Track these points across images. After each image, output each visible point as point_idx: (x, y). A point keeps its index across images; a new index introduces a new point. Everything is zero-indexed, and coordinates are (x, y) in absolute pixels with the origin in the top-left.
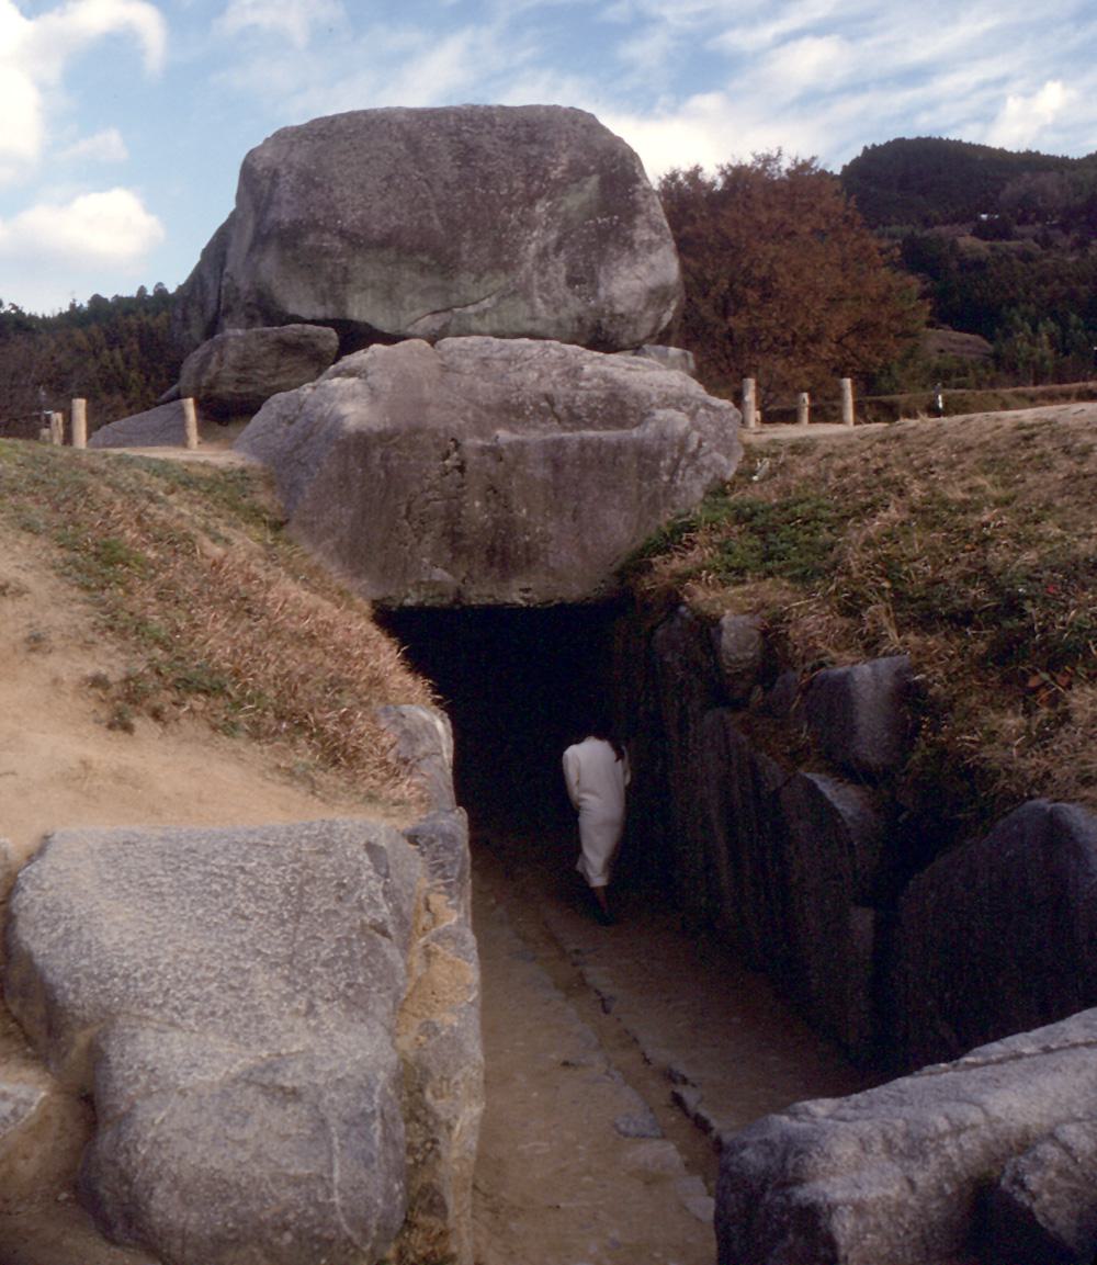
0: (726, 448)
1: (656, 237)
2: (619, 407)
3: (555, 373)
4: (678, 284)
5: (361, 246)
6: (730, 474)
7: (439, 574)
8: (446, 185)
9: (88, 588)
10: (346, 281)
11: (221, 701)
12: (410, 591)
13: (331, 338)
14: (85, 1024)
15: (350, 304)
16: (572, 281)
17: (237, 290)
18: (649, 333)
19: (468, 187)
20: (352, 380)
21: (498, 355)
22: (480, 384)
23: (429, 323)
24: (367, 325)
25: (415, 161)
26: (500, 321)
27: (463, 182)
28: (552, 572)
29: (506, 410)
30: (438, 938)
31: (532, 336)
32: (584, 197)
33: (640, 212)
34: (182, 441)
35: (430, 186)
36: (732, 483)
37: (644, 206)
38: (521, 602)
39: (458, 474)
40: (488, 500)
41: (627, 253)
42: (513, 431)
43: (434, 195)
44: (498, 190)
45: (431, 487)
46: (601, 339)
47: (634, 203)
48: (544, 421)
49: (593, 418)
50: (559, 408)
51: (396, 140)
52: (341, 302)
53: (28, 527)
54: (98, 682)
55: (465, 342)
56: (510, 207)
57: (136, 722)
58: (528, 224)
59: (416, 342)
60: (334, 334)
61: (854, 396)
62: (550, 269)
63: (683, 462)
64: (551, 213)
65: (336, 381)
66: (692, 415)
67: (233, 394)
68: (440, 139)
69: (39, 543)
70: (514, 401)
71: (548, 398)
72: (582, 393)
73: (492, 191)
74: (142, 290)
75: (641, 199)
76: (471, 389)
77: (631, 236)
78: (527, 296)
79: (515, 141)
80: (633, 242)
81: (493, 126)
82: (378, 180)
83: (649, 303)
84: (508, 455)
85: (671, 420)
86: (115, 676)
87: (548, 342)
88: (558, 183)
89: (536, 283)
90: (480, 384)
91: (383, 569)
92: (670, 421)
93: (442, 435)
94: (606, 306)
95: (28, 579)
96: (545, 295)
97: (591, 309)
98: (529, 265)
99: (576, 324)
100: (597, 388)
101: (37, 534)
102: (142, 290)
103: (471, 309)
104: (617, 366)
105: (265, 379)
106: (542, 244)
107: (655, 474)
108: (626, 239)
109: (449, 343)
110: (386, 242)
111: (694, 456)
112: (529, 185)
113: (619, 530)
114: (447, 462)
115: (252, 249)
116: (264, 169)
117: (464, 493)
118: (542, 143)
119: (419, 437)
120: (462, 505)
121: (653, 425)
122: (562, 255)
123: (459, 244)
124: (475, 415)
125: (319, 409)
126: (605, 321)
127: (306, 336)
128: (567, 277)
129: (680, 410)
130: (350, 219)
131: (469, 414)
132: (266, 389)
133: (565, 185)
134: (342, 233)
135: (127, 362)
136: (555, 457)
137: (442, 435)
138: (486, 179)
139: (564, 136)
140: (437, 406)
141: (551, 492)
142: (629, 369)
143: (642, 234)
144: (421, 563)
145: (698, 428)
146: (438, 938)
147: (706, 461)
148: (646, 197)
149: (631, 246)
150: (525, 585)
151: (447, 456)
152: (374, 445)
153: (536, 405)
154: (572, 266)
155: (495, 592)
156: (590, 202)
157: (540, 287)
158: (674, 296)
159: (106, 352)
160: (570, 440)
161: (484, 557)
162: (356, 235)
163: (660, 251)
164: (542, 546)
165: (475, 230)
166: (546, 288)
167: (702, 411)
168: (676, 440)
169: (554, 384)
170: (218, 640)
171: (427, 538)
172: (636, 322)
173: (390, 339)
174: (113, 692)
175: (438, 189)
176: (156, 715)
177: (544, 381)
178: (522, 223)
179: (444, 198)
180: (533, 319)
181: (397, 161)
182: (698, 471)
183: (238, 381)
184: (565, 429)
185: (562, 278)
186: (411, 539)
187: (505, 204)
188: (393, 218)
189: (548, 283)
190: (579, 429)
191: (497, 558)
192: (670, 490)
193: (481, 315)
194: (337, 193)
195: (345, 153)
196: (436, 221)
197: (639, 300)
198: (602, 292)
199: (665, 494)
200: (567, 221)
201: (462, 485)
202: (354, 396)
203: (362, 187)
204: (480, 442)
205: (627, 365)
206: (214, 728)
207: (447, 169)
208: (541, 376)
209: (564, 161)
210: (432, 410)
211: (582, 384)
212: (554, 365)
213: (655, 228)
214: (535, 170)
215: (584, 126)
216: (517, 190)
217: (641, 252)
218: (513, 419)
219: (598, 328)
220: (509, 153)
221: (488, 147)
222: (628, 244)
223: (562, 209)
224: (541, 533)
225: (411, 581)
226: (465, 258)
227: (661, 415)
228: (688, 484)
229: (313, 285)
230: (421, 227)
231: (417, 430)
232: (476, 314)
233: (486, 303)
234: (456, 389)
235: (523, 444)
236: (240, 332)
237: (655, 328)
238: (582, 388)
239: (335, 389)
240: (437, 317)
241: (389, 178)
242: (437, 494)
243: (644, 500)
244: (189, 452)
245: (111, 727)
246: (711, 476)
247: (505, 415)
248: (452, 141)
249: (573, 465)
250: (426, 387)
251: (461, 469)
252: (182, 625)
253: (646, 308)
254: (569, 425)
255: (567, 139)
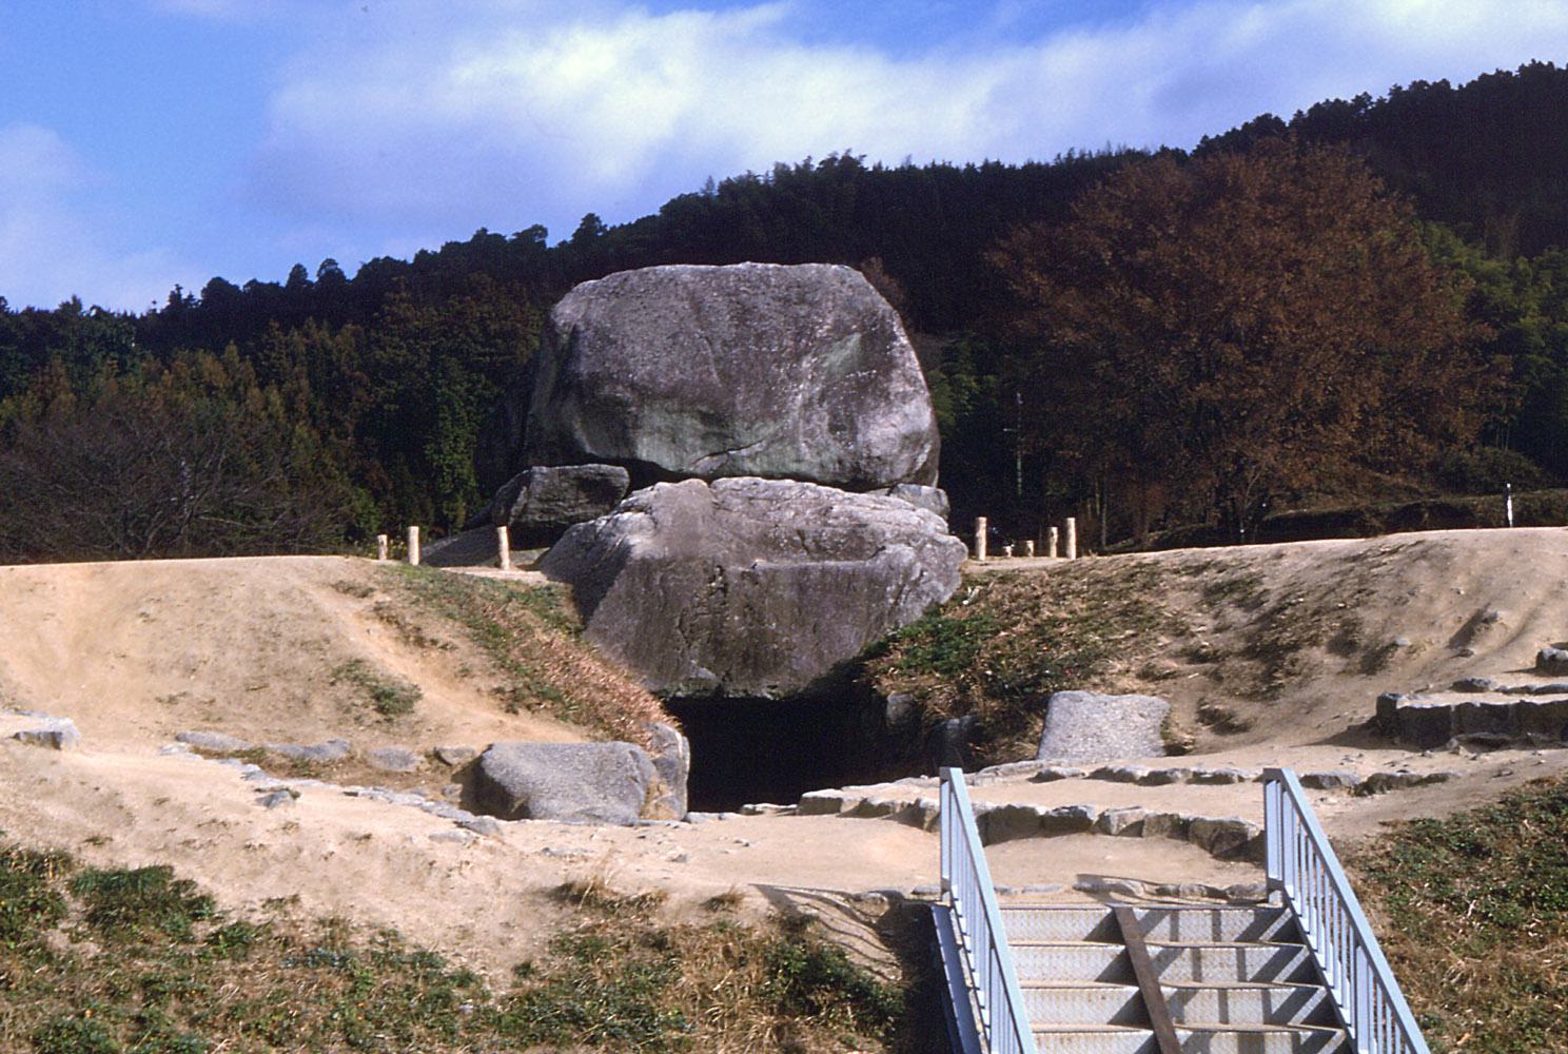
0: (945, 575)
1: (909, 389)
2: (859, 540)
3: (808, 512)
4: (931, 430)
5: (649, 397)
6: (946, 599)
7: (705, 673)
8: (725, 343)
9: (487, 648)
10: (636, 427)
11: (559, 705)
12: (681, 685)
13: (623, 476)
14: (518, 799)
15: (639, 446)
16: (833, 428)
17: (541, 429)
18: (905, 472)
19: (743, 345)
20: (641, 515)
21: (762, 496)
22: (746, 521)
23: (706, 463)
24: (653, 464)
25: (697, 319)
26: (770, 463)
27: (740, 339)
28: (794, 673)
29: (765, 543)
30: (662, 801)
31: (799, 477)
32: (846, 353)
33: (895, 366)
34: (498, 565)
35: (711, 344)
36: (945, 607)
37: (900, 361)
38: (769, 696)
39: (721, 595)
40: (745, 615)
41: (883, 404)
42: (769, 560)
43: (714, 352)
44: (769, 348)
45: (700, 604)
46: (858, 480)
47: (892, 358)
48: (795, 552)
49: (835, 551)
50: (808, 542)
51: (682, 300)
52: (629, 443)
53: (450, 616)
54: (499, 690)
55: (736, 483)
56: (779, 362)
57: (520, 711)
58: (795, 378)
59: (695, 481)
60: (626, 473)
61: (1077, 537)
62: (815, 417)
63: (907, 588)
64: (816, 368)
65: (626, 515)
66: (920, 549)
67: (537, 522)
68: (720, 299)
69: (458, 624)
70: (771, 535)
71: (800, 533)
72: (828, 529)
73: (764, 349)
74: (298, 273)
75: (898, 355)
76: (738, 524)
77: (887, 388)
78: (794, 441)
79: (786, 300)
80: (889, 394)
81: (768, 286)
82: (664, 337)
83: (903, 447)
84: (762, 579)
85: (899, 553)
86: (508, 689)
87: (806, 484)
88: (822, 340)
89: (801, 430)
90: (746, 521)
91: (660, 668)
92: (897, 554)
93: (710, 562)
94: (864, 450)
95: (456, 642)
96: (809, 440)
97: (850, 453)
98: (796, 414)
99: (837, 466)
100: (843, 525)
101: (455, 620)
102: (298, 273)
103: (744, 452)
104: (865, 506)
105: (566, 510)
106: (807, 396)
107: (883, 597)
108: (883, 390)
109: (724, 483)
110: (670, 394)
111: (916, 583)
112: (797, 342)
113: (851, 642)
114: (713, 584)
115: (553, 398)
116: (565, 324)
117: (727, 609)
118: (811, 304)
119: (693, 564)
120: (723, 619)
121: (883, 557)
122: (825, 404)
123: (734, 397)
124: (738, 546)
125: (613, 539)
126: (863, 462)
127: (602, 475)
128: (830, 425)
129: (909, 545)
130: (641, 373)
131: (733, 546)
132: (567, 518)
133: (830, 342)
134: (633, 386)
135: (290, 407)
136: (800, 579)
137: (710, 562)
138: (759, 337)
139: (831, 297)
140: (707, 538)
141: (796, 610)
142: (875, 508)
143: (897, 386)
144: (690, 664)
145: (923, 560)
146: (662, 801)
147: (926, 588)
148: (902, 352)
149: (887, 398)
150: (772, 683)
151: (713, 579)
152: (655, 570)
153: (790, 538)
154: (834, 415)
155: (749, 688)
156: (852, 357)
157: (805, 434)
158: (927, 441)
159: (256, 391)
160: (813, 568)
161: (740, 660)
162: (645, 387)
163: (914, 402)
164: (786, 653)
165: (748, 383)
166: (811, 434)
167: (929, 546)
168: (902, 570)
169: (807, 521)
170: (554, 676)
171: (696, 644)
172: (891, 464)
173: (676, 477)
174: (507, 695)
175: (718, 346)
176: (528, 707)
177: (799, 519)
178: (790, 378)
179: (722, 355)
180: (798, 461)
181: (682, 319)
182: (919, 596)
183: (542, 511)
184: (813, 559)
185: (825, 425)
186: (683, 644)
187: (775, 361)
188: (677, 372)
189: (813, 430)
190: (824, 559)
191: (750, 661)
192: (895, 610)
193: (752, 458)
194: (629, 349)
195: (635, 311)
196: (715, 376)
197: (893, 446)
198: (860, 437)
199: (889, 614)
200: (830, 375)
201: (724, 603)
202: (641, 528)
203: (651, 343)
204: (741, 569)
205: (873, 505)
206: (557, 717)
207: (725, 326)
208: (796, 514)
209: (829, 321)
210: (703, 542)
211: (830, 521)
212: (808, 506)
213: (911, 381)
214: (803, 331)
215: (850, 286)
216: (787, 347)
217: (896, 402)
218: (770, 550)
219: (856, 469)
220: (780, 312)
221: (763, 308)
222: (885, 395)
223: (826, 365)
224: (787, 642)
225: (682, 678)
226: (739, 408)
227: (891, 549)
228: (909, 606)
229: (608, 430)
230: (701, 380)
231: (689, 558)
232: (749, 457)
233: (757, 447)
234: (725, 525)
235: (776, 571)
236: (545, 469)
237: (911, 469)
238: (829, 525)
239: (625, 522)
240: (715, 458)
241: (675, 336)
242: (704, 610)
243: (873, 618)
244: (501, 572)
245: (507, 711)
246: (929, 600)
247: (764, 547)
248: (731, 301)
249: (815, 590)
250: (700, 523)
251: (724, 590)
252: (538, 668)
253: (900, 451)
254: (816, 556)
255: (833, 301)
